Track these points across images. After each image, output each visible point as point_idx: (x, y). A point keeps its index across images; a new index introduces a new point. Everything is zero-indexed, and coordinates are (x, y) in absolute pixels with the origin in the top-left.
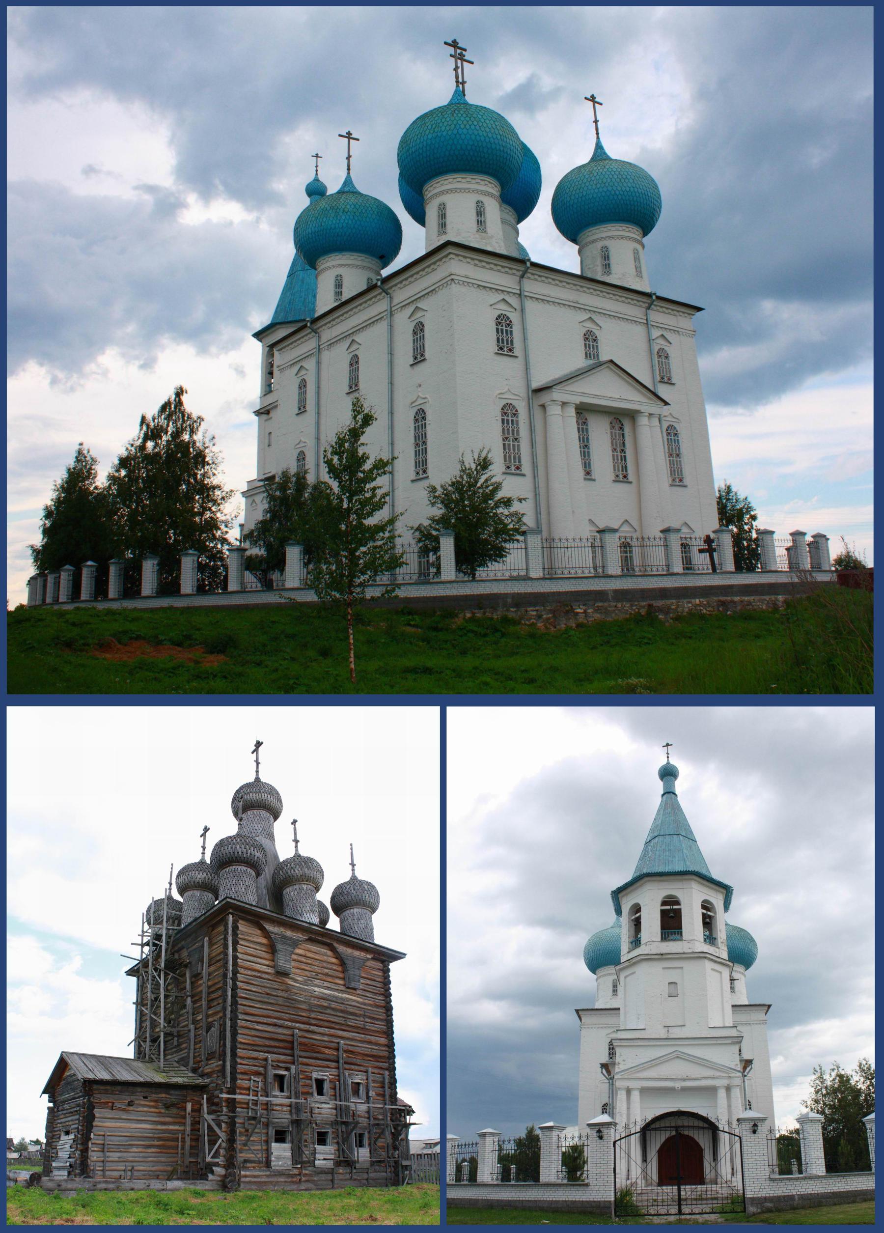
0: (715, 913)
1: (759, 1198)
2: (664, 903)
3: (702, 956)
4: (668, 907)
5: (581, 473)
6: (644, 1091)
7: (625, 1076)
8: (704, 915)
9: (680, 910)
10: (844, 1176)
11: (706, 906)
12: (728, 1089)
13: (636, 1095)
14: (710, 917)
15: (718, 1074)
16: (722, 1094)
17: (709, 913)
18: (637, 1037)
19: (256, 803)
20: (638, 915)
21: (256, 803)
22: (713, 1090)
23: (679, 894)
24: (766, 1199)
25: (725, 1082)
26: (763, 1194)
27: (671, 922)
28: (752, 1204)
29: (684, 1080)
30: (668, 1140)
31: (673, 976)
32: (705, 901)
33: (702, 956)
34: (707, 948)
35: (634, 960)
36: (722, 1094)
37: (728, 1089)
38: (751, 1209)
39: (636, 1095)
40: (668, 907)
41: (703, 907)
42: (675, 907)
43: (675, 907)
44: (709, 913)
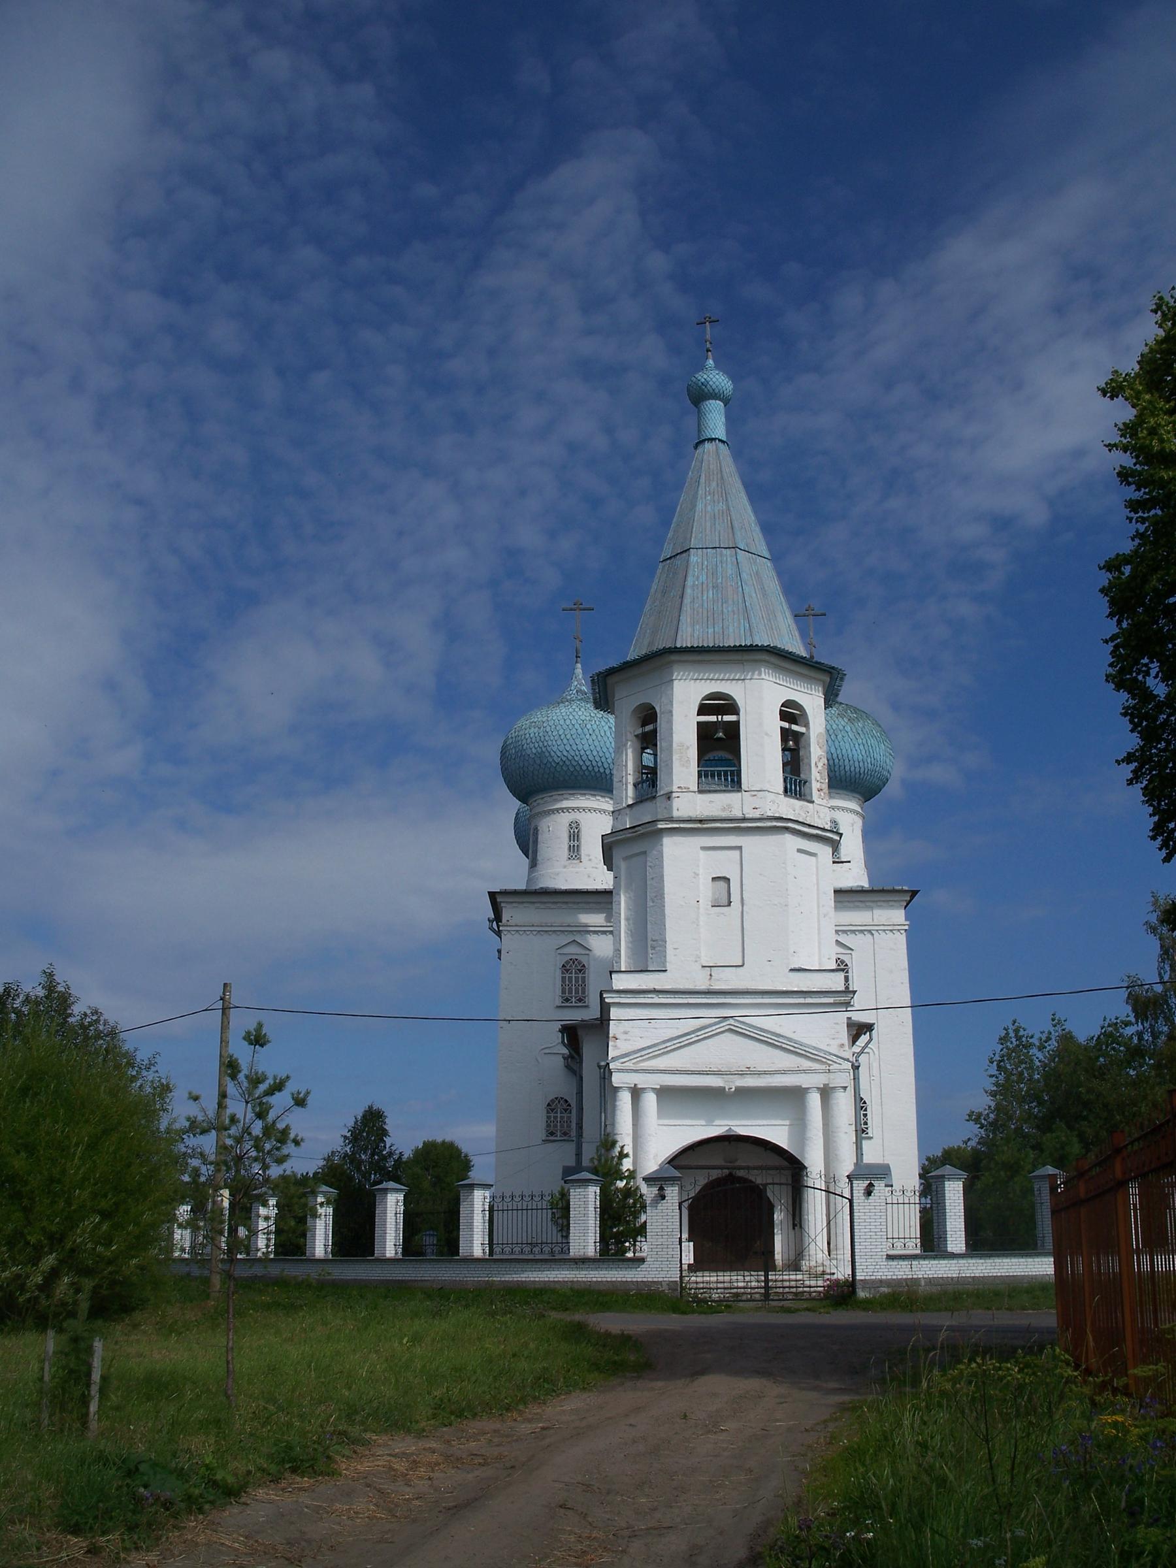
0: (807, 725)
1: (873, 1281)
2: (703, 710)
3: (778, 826)
4: (713, 718)
5: (662, 974)
6: (664, 1093)
7: (629, 1065)
8: (786, 734)
9: (736, 725)
10: (990, 1256)
11: (791, 713)
12: (826, 1093)
13: (650, 1101)
14: (797, 736)
15: (807, 1064)
16: (814, 1100)
17: (795, 727)
18: (651, 986)
19: (260, 1025)
20: (649, 728)
21: (260, 1025)
22: (796, 1095)
23: (733, 689)
24: (881, 1282)
25: (819, 1080)
26: (879, 1275)
27: (720, 747)
28: (864, 1288)
29: (741, 1074)
30: (711, 1186)
31: (725, 863)
32: (788, 704)
33: (778, 826)
34: (790, 808)
35: (642, 830)
36: (814, 1100)
37: (826, 1093)
38: (862, 1294)
39: (650, 1101)
40: (713, 718)
41: (784, 716)
42: (727, 718)
43: (727, 718)
44: (795, 727)
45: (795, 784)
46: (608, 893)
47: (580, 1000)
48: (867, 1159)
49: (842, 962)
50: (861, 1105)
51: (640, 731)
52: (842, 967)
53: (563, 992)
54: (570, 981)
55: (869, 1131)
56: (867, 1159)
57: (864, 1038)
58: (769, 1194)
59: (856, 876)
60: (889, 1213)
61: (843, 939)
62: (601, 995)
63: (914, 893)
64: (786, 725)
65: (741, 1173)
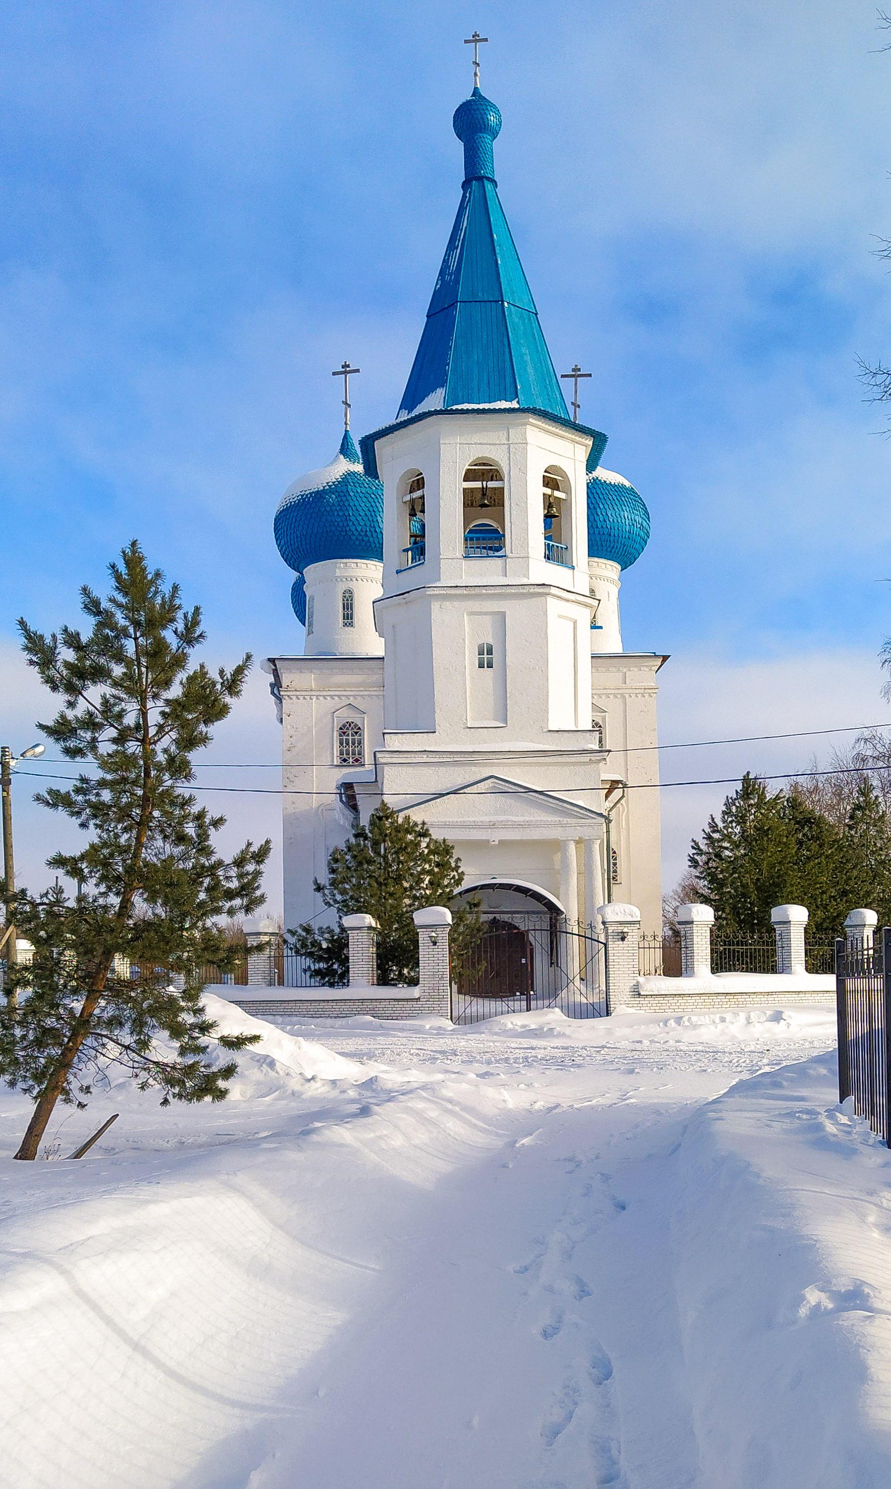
2: (469, 476)
4: (478, 485)
9: (423, 478)
17: (557, 494)
20: (418, 494)
41: (549, 482)
42: (491, 484)
43: (491, 484)
44: (557, 494)
45: (556, 553)
46: (383, 658)
47: (357, 760)
48: (386, 768)
49: (597, 724)
50: (611, 856)
51: (408, 498)
52: (598, 727)
53: (341, 753)
54: (348, 744)
55: (618, 878)
56: (386, 768)
57: (617, 793)
58: (531, 938)
59: (612, 643)
60: (641, 958)
61: (600, 703)
62: (375, 753)
63: (665, 658)
64: (548, 491)
65: (505, 918)
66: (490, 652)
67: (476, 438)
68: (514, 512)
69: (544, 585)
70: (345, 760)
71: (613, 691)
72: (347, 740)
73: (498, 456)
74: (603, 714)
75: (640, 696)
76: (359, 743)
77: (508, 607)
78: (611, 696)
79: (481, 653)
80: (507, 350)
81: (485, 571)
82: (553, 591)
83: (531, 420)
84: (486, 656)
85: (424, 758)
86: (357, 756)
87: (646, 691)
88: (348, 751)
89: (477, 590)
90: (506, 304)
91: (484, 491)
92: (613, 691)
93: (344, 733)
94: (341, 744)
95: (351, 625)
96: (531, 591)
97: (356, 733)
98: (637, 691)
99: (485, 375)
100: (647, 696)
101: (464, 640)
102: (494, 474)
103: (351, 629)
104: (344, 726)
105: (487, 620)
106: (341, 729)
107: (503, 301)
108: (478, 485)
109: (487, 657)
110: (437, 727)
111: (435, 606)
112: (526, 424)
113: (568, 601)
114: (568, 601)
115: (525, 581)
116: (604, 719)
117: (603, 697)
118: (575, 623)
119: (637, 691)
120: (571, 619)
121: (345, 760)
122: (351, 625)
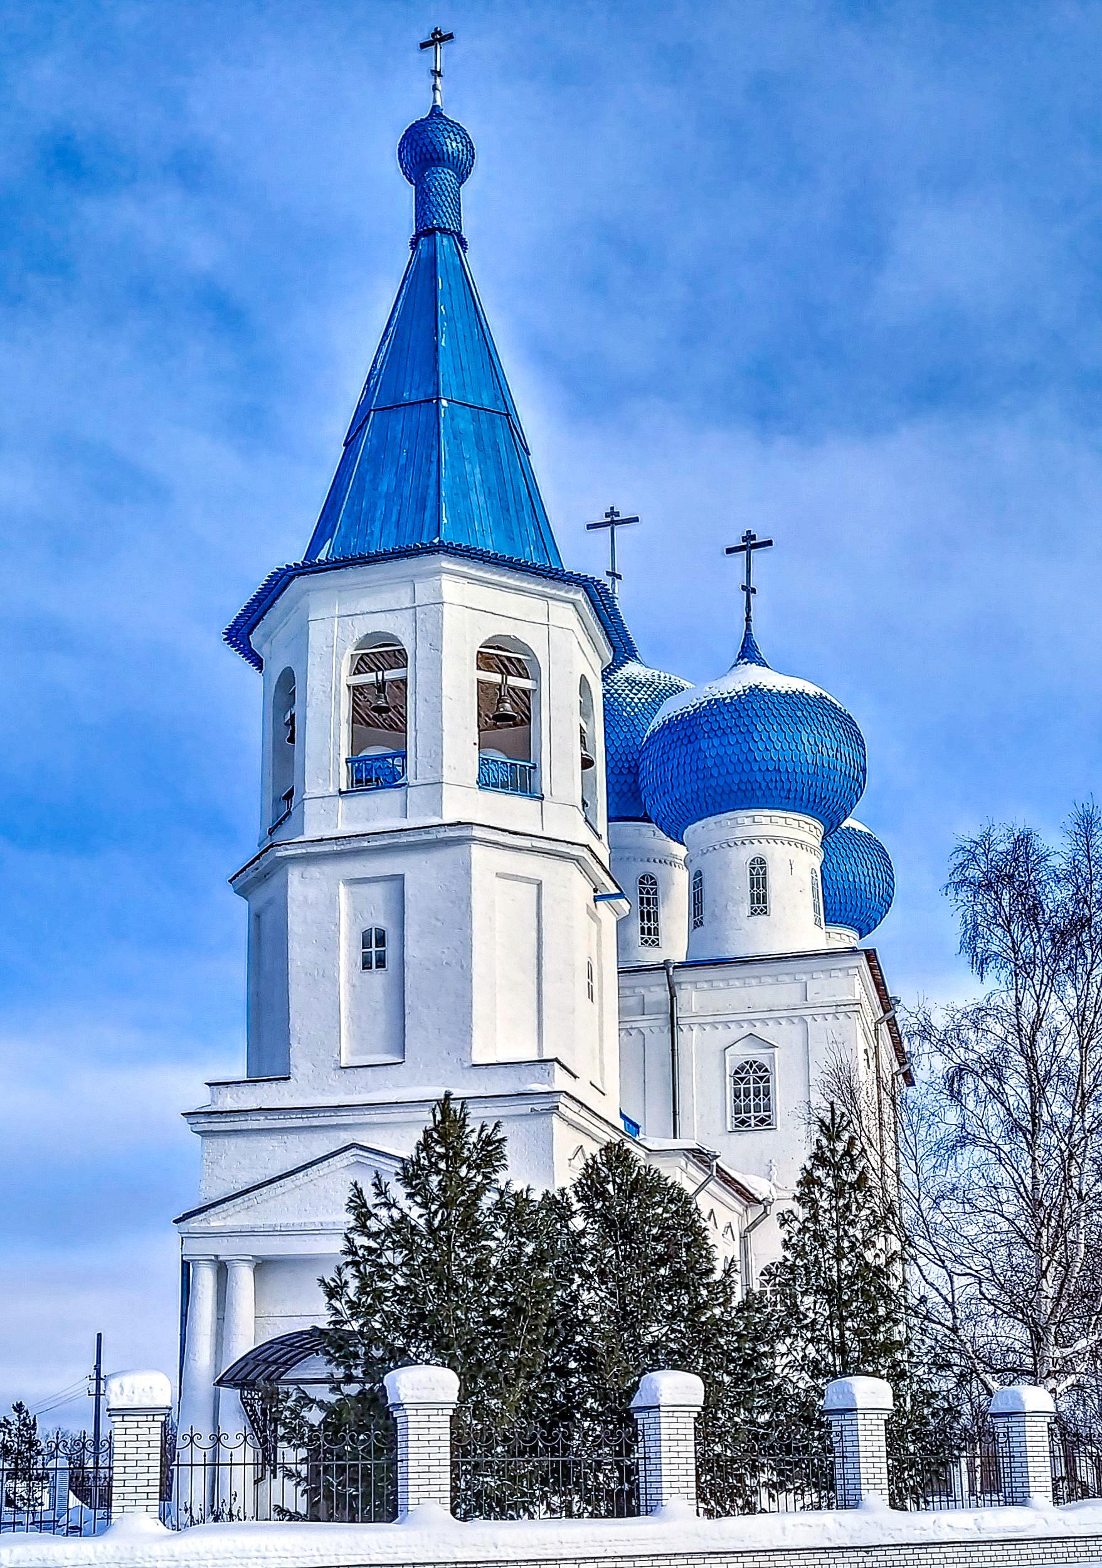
4: (369, 678)
47: (762, 1121)
66: (381, 941)
67: (365, 605)
68: (420, 714)
69: (459, 823)
70: (743, 1122)
71: (785, 1014)
72: (747, 1090)
73: (399, 627)
74: (771, 1050)
75: (829, 1017)
76: (767, 1094)
77: (410, 866)
78: (783, 1022)
79: (366, 944)
80: (434, 467)
81: (379, 812)
82: (477, 832)
83: (444, 564)
84: (374, 949)
85: (263, 1122)
86: (762, 1114)
87: (840, 1009)
88: (747, 1106)
89: (355, 844)
90: (444, 403)
91: (381, 686)
92: (785, 1014)
93: (742, 1079)
94: (737, 1096)
95: (764, 912)
96: (441, 836)
97: (761, 1078)
98: (826, 1010)
99: (395, 512)
100: (841, 1016)
101: (337, 925)
102: (399, 658)
103: (765, 917)
104: (742, 1068)
105: (377, 892)
106: (736, 1073)
107: (439, 399)
108: (369, 678)
109: (376, 950)
110: (293, 1070)
111: (294, 875)
112: (441, 571)
113: (519, 849)
114: (519, 849)
115: (436, 821)
116: (772, 1058)
117: (829, 1017)
118: (539, 885)
119: (826, 1010)
120: (529, 880)
121: (743, 1122)
122: (764, 912)
